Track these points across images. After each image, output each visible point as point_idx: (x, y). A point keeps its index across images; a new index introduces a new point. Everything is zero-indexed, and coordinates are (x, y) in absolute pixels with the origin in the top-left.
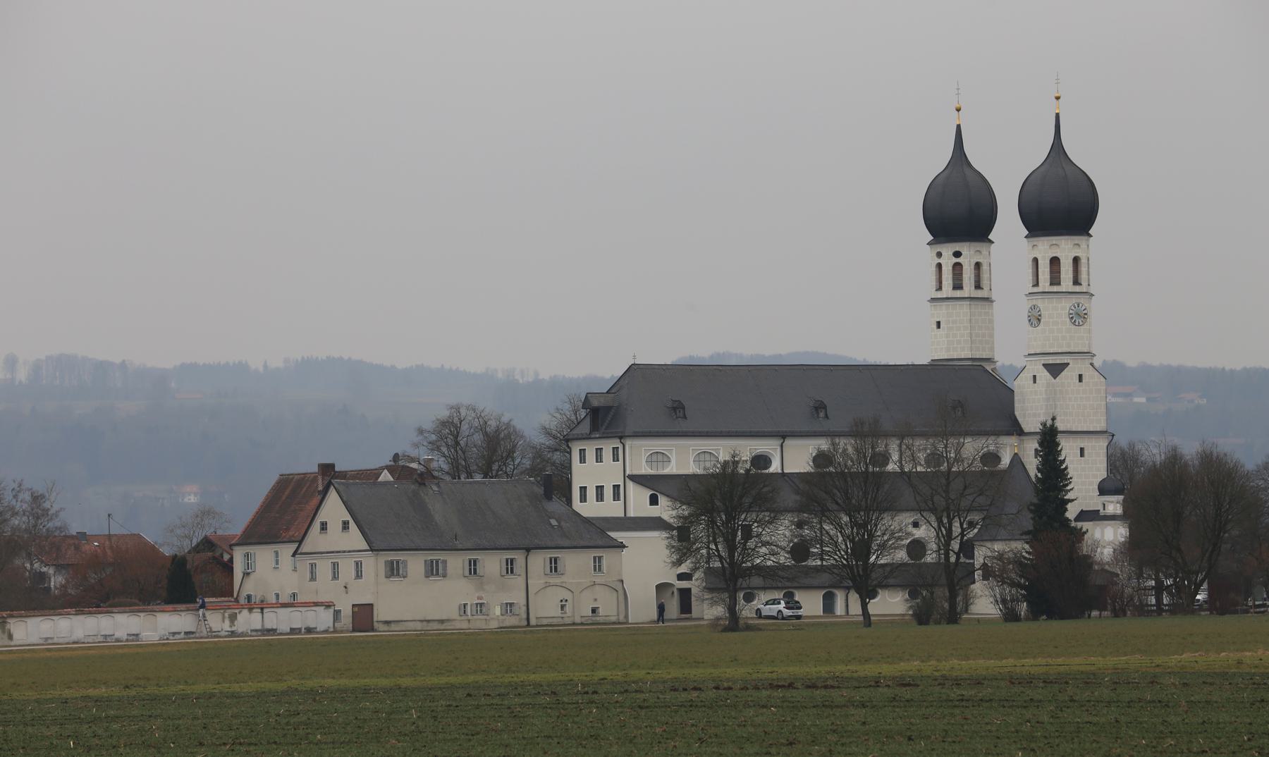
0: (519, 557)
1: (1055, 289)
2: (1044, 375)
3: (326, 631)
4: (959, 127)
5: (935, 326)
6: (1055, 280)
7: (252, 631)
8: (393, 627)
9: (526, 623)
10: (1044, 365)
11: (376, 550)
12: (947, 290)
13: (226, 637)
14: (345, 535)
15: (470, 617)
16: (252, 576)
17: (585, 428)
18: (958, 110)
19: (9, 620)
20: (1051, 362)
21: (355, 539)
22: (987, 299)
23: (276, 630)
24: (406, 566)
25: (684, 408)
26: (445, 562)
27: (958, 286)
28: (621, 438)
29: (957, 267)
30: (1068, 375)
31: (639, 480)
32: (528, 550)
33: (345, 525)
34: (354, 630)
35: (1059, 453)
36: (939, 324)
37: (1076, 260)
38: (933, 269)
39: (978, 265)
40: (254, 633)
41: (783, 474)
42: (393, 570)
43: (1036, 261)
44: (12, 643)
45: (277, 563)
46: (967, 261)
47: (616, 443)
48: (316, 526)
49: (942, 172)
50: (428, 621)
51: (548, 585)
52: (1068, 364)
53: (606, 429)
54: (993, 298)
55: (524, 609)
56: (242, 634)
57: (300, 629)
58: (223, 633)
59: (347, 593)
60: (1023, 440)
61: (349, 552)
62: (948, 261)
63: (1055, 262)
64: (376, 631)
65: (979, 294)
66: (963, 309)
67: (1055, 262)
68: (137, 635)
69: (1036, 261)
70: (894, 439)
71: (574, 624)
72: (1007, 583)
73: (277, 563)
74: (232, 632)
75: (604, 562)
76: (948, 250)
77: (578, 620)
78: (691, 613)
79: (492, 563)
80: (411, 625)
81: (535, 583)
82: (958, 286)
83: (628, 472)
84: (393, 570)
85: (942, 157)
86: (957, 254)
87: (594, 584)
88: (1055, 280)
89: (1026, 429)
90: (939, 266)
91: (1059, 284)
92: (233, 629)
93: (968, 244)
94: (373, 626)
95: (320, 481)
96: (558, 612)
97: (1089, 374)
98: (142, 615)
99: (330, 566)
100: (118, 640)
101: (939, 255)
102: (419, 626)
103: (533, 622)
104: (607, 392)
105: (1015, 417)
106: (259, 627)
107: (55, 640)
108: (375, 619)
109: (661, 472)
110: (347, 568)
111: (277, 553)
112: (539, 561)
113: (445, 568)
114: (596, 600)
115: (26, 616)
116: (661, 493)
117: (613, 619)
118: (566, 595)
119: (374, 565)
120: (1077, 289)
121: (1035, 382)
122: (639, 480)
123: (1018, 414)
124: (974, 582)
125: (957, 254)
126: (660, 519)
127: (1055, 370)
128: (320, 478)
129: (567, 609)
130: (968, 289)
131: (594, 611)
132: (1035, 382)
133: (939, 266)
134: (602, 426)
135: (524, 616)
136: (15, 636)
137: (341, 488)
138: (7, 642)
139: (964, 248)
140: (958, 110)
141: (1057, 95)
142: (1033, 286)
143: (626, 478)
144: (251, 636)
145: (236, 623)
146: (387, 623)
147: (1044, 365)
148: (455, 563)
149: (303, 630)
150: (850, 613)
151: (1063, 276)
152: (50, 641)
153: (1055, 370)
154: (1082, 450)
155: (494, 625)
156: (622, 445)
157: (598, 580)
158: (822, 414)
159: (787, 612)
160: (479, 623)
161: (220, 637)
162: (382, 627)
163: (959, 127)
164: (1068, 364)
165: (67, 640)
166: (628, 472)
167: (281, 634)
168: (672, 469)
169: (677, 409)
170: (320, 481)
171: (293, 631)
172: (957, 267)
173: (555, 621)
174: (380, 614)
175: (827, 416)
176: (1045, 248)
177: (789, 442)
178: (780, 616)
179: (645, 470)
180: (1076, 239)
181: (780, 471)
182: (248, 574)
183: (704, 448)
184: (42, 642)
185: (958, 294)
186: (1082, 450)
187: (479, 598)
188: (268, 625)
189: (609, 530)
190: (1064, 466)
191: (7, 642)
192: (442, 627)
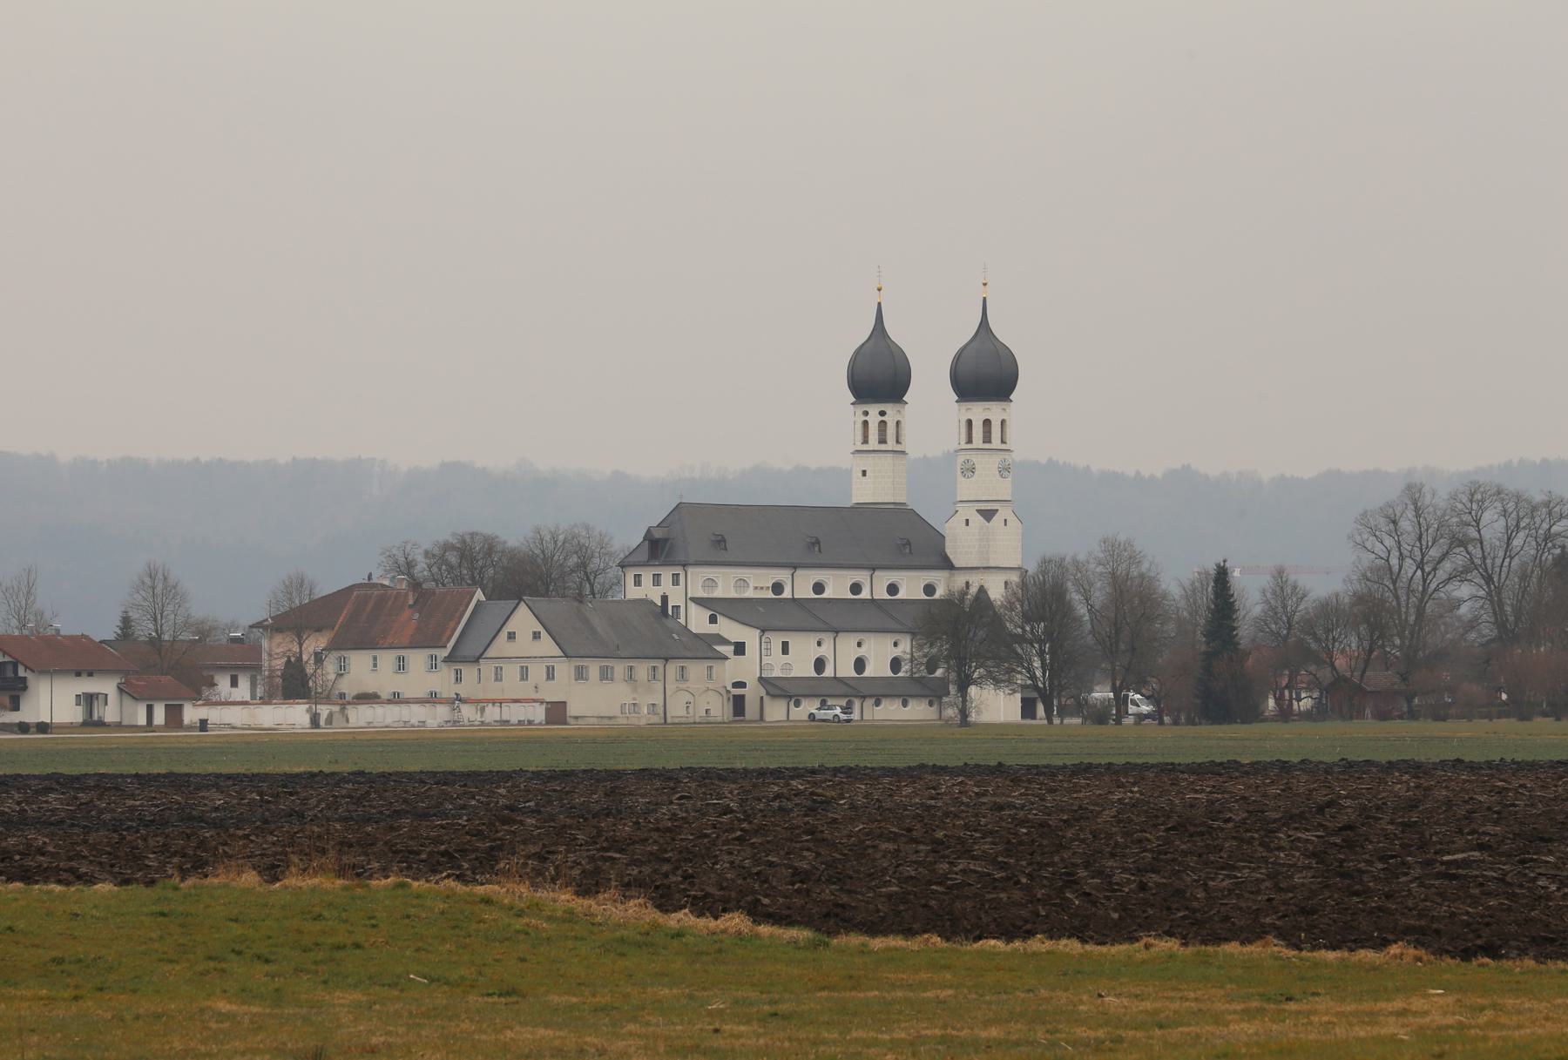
0: (659, 664)
1: (987, 446)
2: (977, 520)
3: (540, 724)
4: (879, 304)
5: (861, 474)
6: (987, 438)
7: (495, 721)
8: (580, 722)
9: (663, 721)
10: (978, 511)
11: (570, 657)
12: (873, 442)
13: (479, 726)
14: (537, 643)
15: (628, 715)
16: (346, 676)
17: (644, 555)
18: (879, 290)
19: (347, 707)
20: (983, 508)
21: (547, 646)
22: (903, 452)
23: (508, 721)
24: (587, 671)
25: (725, 541)
26: (612, 668)
27: (882, 441)
28: (684, 566)
29: (883, 424)
30: (997, 519)
31: (699, 601)
32: (667, 660)
33: (536, 636)
34: (548, 723)
35: (1229, 589)
37: (1003, 422)
38: (859, 426)
39: (898, 423)
40: (496, 724)
41: (794, 600)
42: (580, 674)
43: (970, 422)
44: (350, 725)
45: (375, 665)
46: (890, 419)
47: (679, 570)
48: (504, 634)
49: (867, 341)
50: (602, 717)
51: (679, 690)
52: (997, 510)
53: (665, 557)
54: (907, 451)
55: (662, 709)
56: (488, 725)
57: (524, 721)
58: (477, 723)
59: (537, 692)
61: (541, 657)
62: (874, 419)
63: (987, 423)
64: (569, 725)
67: (987, 423)
68: (424, 722)
69: (970, 422)
71: (695, 723)
72: (1303, 688)
73: (375, 665)
74: (482, 722)
75: (714, 670)
76: (874, 410)
77: (698, 720)
78: (744, 715)
79: (642, 669)
80: (592, 721)
81: (671, 687)
82: (882, 441)
83: (689, 595)
84: (580, 674)
85: (966, 332)
86: (882, 413)
87: (708, 689)
88: (987, 438)
89: (957, 563)
90: (865, 423)
91: (990, 442)
92: (483, 719)
93: (892, 405)
94: (566, 719)
95: (411, 597)
96: (683, 713)
97: (1012, 520)
98: (427, 705)
100: (413, 726)
101: (866, 413)
102: (595, 721)
103: (669, 721)
104: (657, 526)
105: (946, 555)
106: (499, 719)
107: (376, 725)
108: (568, 714)
109: (711, 596)
110: (537, 672)
111: (375, 659)
112: (673, 668)
113: (612, 673)
114: (708, 703)
115: (359, 704)
116: (719, 613)
117: (720, 719)
119: (564, 669)
120: (883, 447)
121: (1005, 525)
122: (699, 601)
123: (948, 551)
125: (882, 413)
126: (718, 635)
127: (988, 515)
128: (411, 594)
129: (691, 710)
130: (891, 444)
131: (707, 711)
132: (1005, 525)
133: (865, 423)
134: (661, 554)
135: (662, 715)
136: (350, 720)
137: (530, 603)
138: (345, 725)
139: (890, 408)
140: (879, 290)
141: (984, 282)
142: (966, 443)
143: (688, 600)
144: (418, 726)
145: (485, 714)
146: (576, 718)
147: (978, 511)
148: (620, 668)
149: (526, 722)
150: (791, 718)
151: (993, 435)
152: (371, 725)
153: (988, 515)
155: (643, 722)
156: (684, 572)
157: (711, 686)
158: (817, 549)
160: (634, 721)
161: (474, 726)
163: (879, 304)
164: (997, 510)
165: (381, 725)
166: (689, 595)
167: (512, 725)
168: (718, 593)
169: (720, 542)
170: (411, 597)
172: (883, 424)
173: (682, 720)
174: (572, 710)
175: (820, 551)
177: (799, 572)
178: (836, 720)
179: (701, 594)
181: (869, 597)
182: (342, 675)
183: (740, 576)
184: (366, 725)
185: (883, 447)
187: (634, 699)
188: (504, 718)
189: (716, 644)
190: (1232, 600)
191: (345, 725)
192: (611, 723)
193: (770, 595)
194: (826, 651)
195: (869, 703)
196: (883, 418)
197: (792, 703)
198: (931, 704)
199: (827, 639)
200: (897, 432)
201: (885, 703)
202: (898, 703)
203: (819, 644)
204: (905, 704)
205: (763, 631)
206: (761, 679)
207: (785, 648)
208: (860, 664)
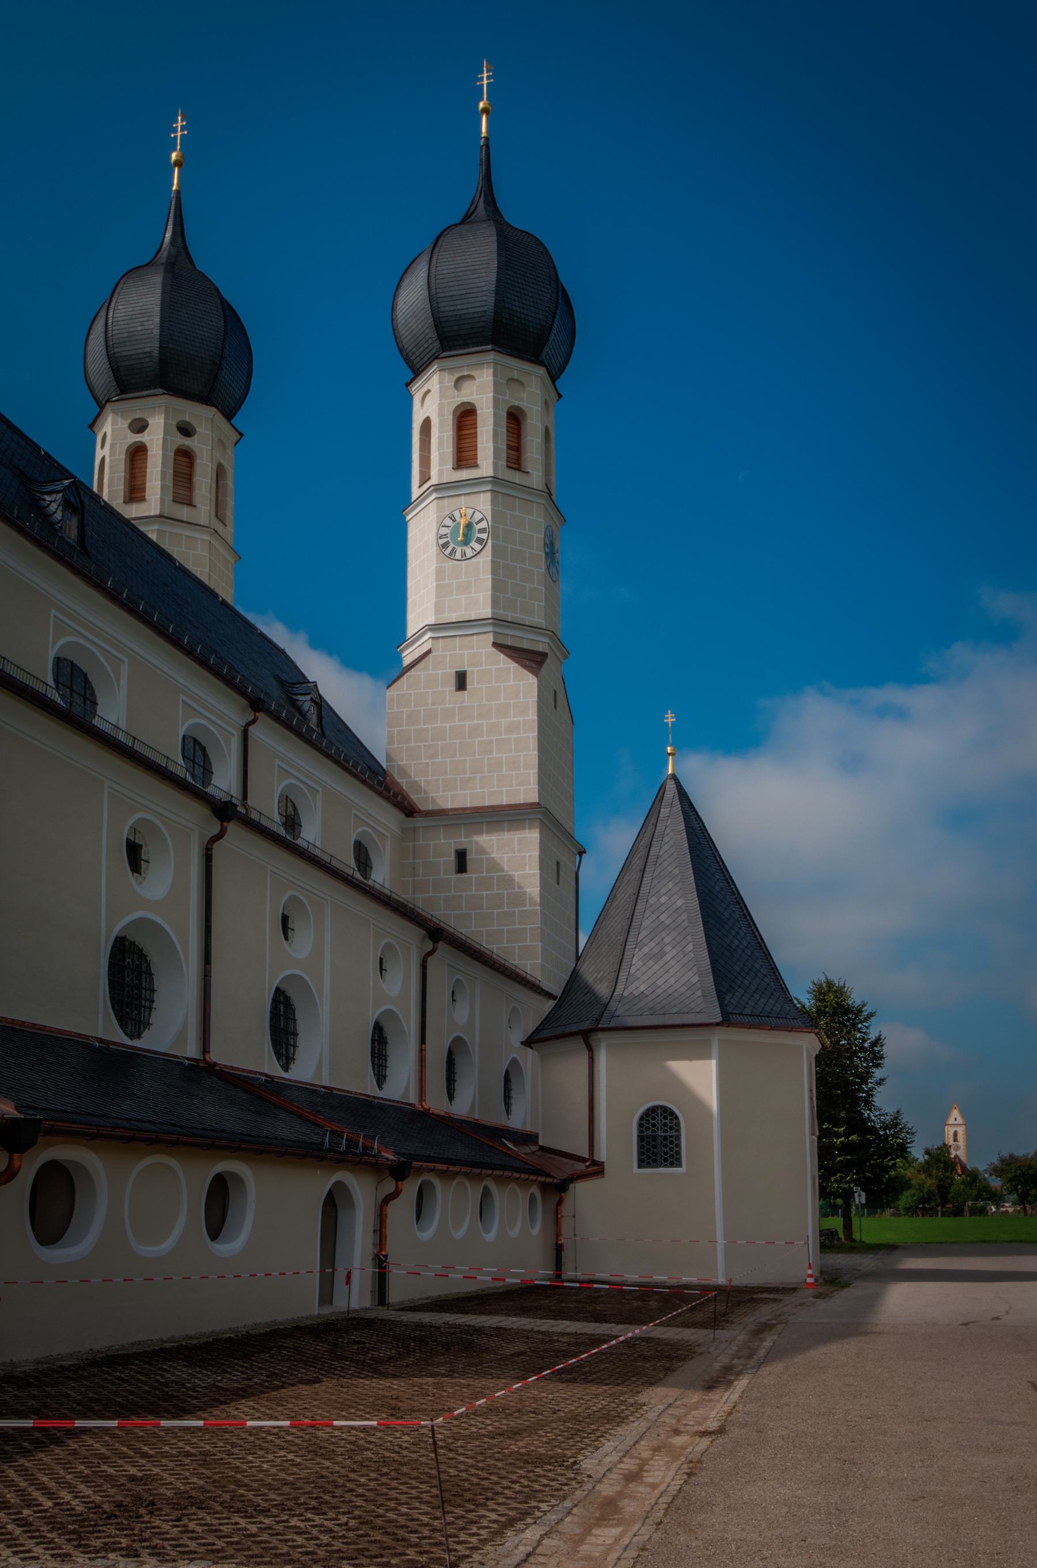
10: (495, 645)
60: (415, 830)
133: (137, 454)
196: (187, 442)
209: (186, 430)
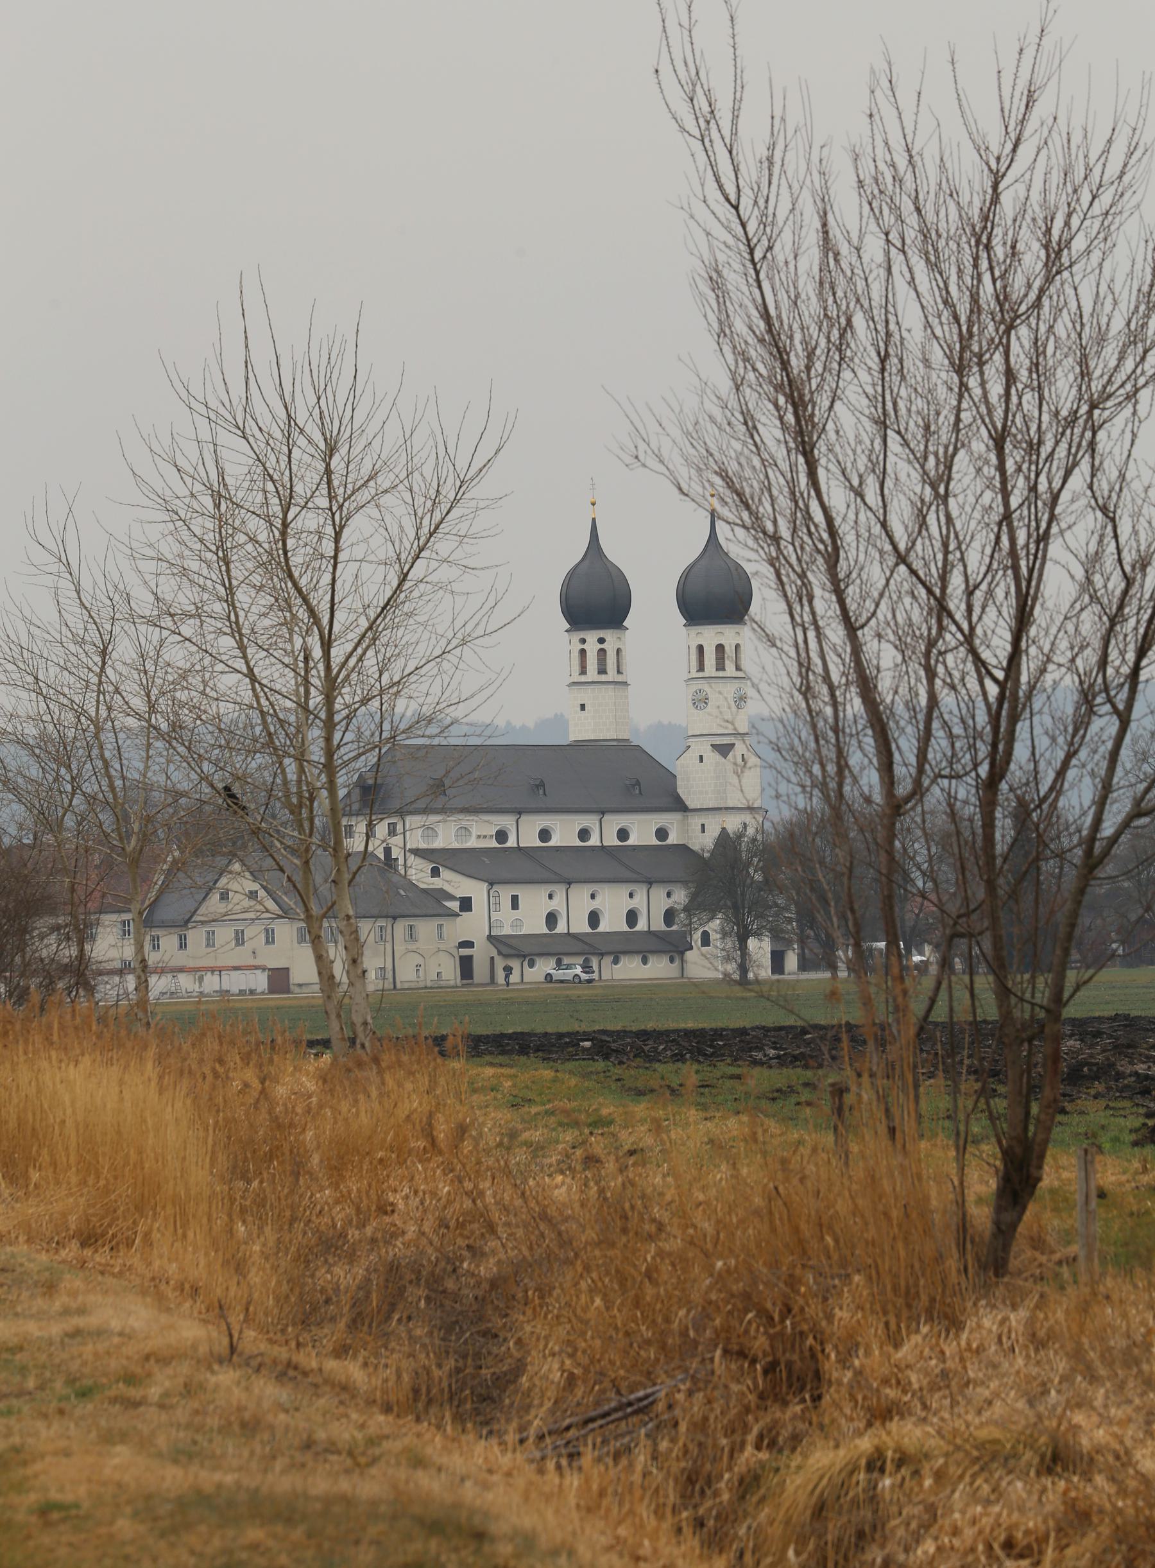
1: (721, 674)
2: (712, 757)
3: (263, 993)
4: (594, 520)
8: (304, 990)
12: (694, 674)
22: (625, 683)
27: (602, 671)
29: (602, 652)
32: (395, 918)
34: (271, 991)
36: (583, 707)
39: (618, 651)
41: (519, 848)
43: (701, 649)
51: (408, 951)
62: (592, 648)
63: (720, 648)
65: (620, 678)
66: (610, 690)
67: (720, 648)
69: (701, 649)
70: (360, 818)
75: (445, 929)
76: (592, 637)
77: (429, 984)
81: (400, 948)
82: (602, 671)
83: (408, 847)
86: (601, 641)
89: (691, 804)
90: (583, 652)
99: (204, 935)
103: (399, 986)
112: (401, 927)
118: (420, 961)
120: (603, 678)
124: (691, 948)
125: (601, 641)
129: (421, 973)
130: (612, 675)
133: (583, 652)
139: (608, 635)
146: (300, 985)
154: (703, 826)
157: (442, 947)
159: (584, 976)
162: (297, 990)
166: (408, 847)
171: (242, 993)
172: (602, 652)
173: (413, 985)
176: (710, 636)
180: (737, 628)
185: (603, 678)
186: (703, 826)
193: (494, 844)
194: (558, 904)
195: (608, 960)
197: (526, 964)
198: (672, 960)
199: (560, 891)
200: (719, 809)
201: (624, 960)
202: (638, 959)
203: (550, 897)
204: (645, 961)
205: (491, 884)
206: (490, 938)
207: (515, 904)
208: (594, 918)
209: (583, 641)
